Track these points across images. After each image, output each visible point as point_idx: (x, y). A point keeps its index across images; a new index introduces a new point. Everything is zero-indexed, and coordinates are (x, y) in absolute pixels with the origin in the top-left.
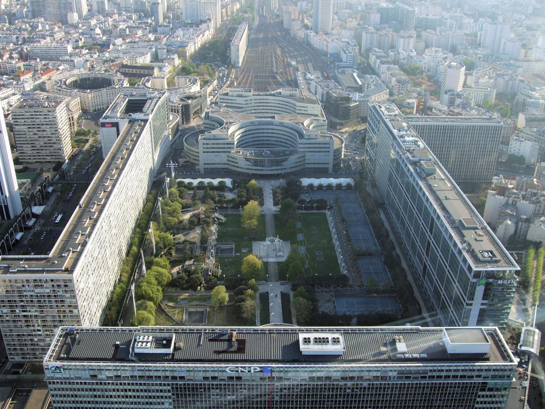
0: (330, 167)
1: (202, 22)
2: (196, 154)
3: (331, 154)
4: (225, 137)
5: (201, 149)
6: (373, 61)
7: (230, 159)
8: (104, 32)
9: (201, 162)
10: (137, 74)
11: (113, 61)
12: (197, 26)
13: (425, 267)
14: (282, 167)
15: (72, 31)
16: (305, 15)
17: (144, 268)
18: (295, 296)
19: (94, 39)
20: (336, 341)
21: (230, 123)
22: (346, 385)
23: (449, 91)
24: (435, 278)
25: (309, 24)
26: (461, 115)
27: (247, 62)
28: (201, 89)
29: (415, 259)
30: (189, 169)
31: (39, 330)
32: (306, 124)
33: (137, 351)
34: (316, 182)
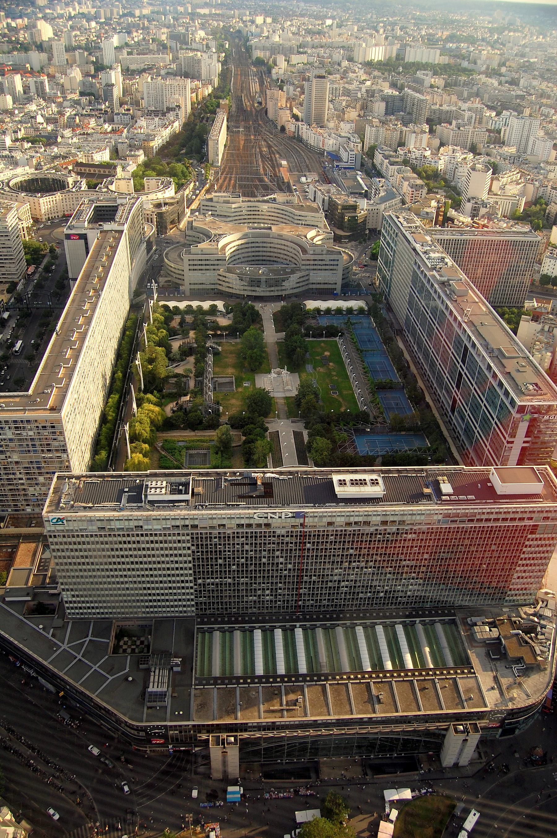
0: (339, 287)
1: (169, 109)
2: (181, 272)
3: (340, 273)
4: (214, 252)
5: (186, 267)
6: (380, 161)
7: (221, 278)
8: (48, 120)
9: (186, 282)
10: (97, 175)
11: (64, 157)
12: (164, 114)
13: (455, 401)
14: (283, 288)
15: (8, 120)
16: (293, 103)
17: (134, 405)
18: (310, 435)
19: (37, 129)
20: (374, 483)
21: (220, 235)
22: (385, 530)
23: (473, 198)
24: (467, 413)
25: (299, 114)
26: (487, 227)
27: (227, 160)
28: (176, 193)
29: (442, 393)
30: (173, 289)
31: (21, 479)
32: (309, 236)
33: (150, 498)
34: (323, 305)
